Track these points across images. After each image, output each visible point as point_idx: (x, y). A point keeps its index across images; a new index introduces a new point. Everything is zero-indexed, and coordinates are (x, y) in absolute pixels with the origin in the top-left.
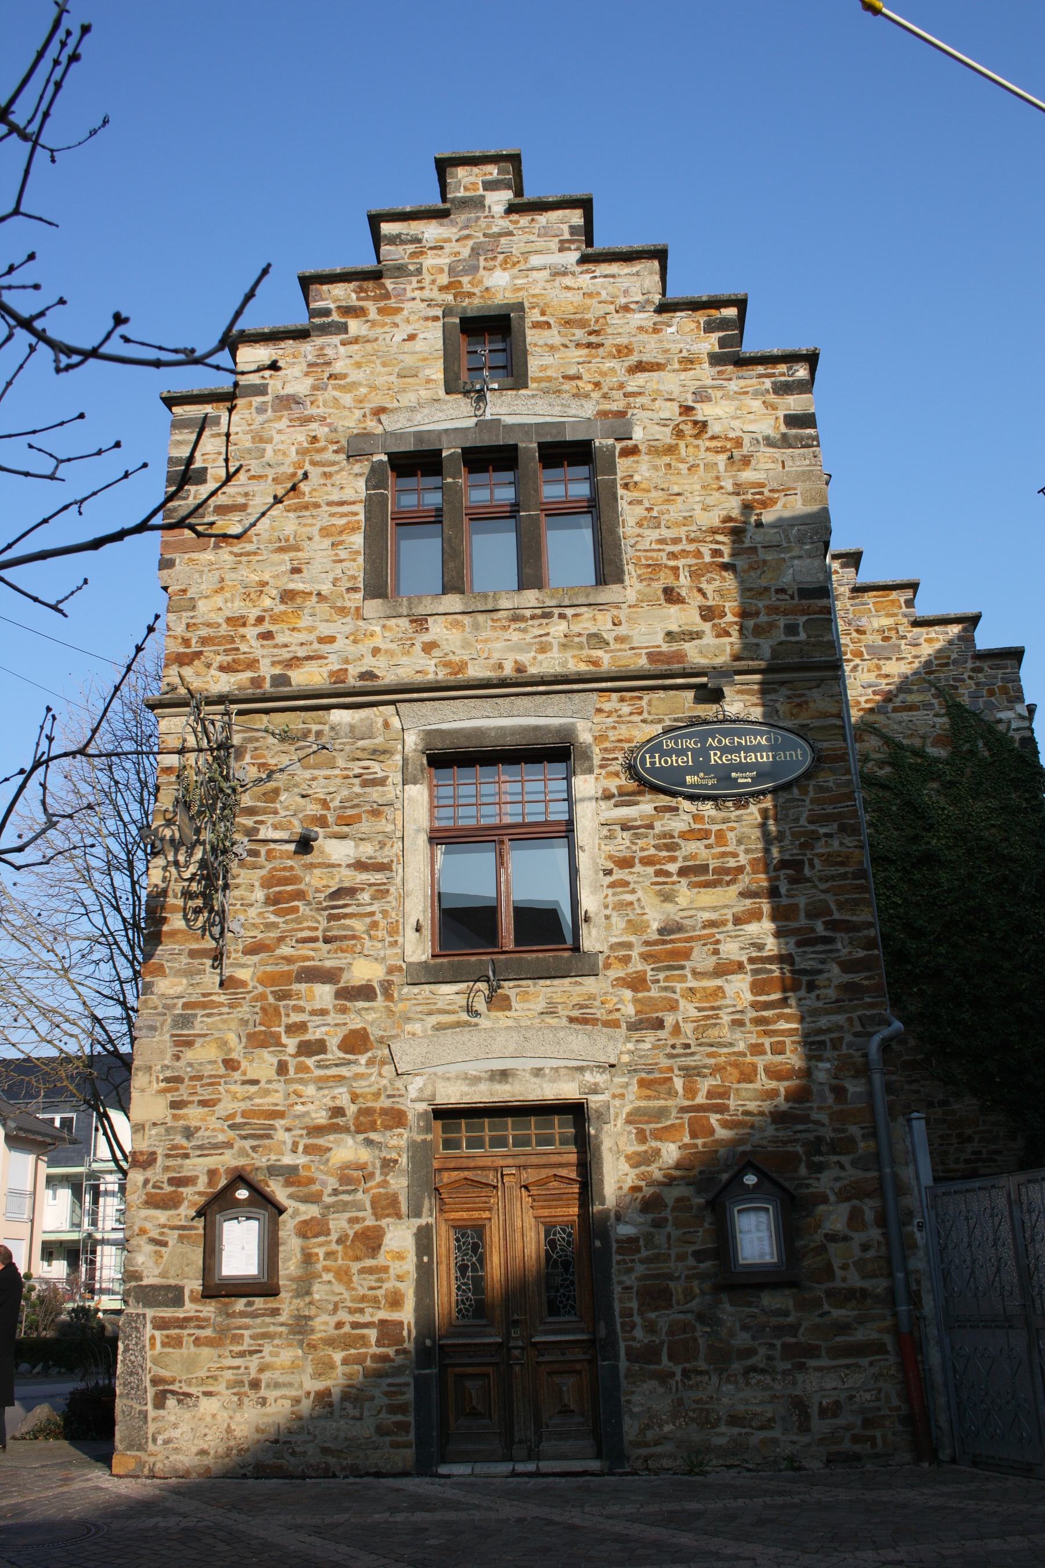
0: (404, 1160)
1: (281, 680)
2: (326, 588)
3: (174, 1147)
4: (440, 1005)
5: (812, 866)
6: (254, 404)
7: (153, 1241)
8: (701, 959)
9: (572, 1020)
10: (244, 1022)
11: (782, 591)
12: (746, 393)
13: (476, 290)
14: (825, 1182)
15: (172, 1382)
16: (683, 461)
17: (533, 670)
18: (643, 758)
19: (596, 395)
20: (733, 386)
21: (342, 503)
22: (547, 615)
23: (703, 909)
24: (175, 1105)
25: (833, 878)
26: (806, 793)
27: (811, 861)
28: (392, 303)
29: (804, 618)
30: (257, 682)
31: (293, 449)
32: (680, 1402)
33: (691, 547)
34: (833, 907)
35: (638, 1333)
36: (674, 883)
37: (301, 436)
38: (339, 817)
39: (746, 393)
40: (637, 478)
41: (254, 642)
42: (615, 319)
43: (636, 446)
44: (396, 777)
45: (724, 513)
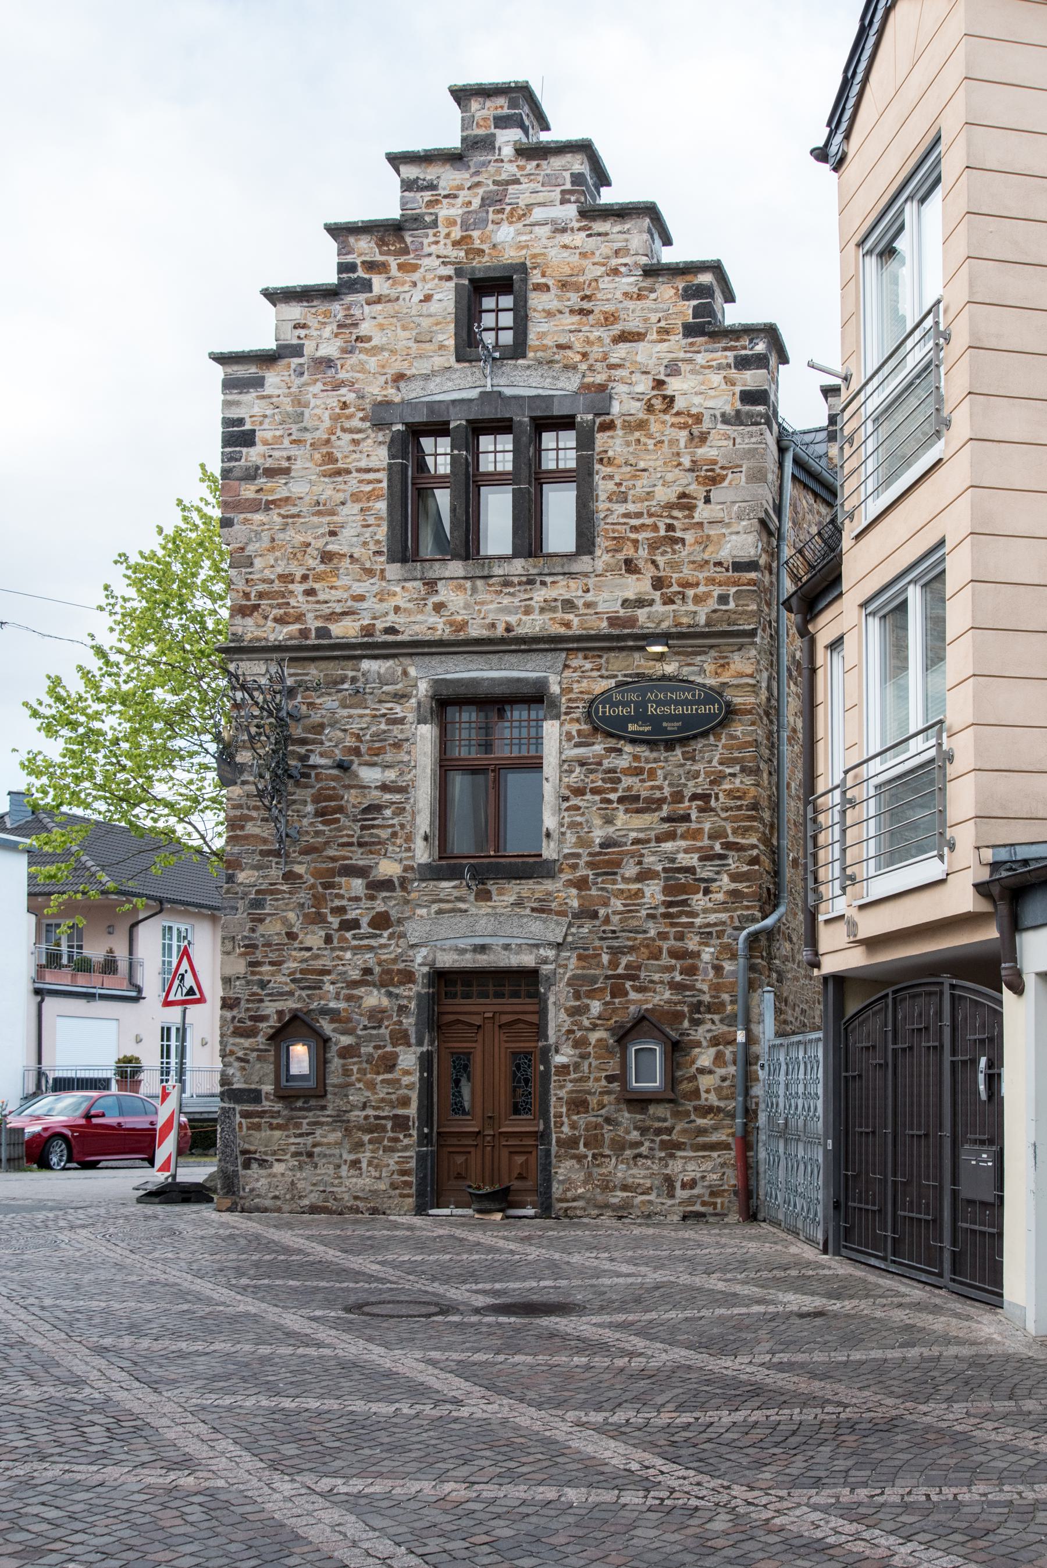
0: (413, 1006)
1: (323, 633)
2: (357, 552)
3: (254, 994)
4: (442, 896)
5: (717, 799)
6: (293, 366)
7: (239, 1059)
8: (630, 870)
9: (533, 910)
10: (302, 906)
11: (719, 564)
12: (710, 367)
13: (484, 247)
14: (701, 1033)
15: (255, 1152)
16: (650, 436)
17: (520, 631)
18: (597, 708)
19: (583, 367)
20: (701, 359)
21: (368, 470)
22: (531, 582)
23: (632, 830)
24: (252, 964)
25: (731, 809)
26: (719, 740)
27: (717, 794)
28: (410, 258)
29: (734, 589)
30: (304, 633)
31: (327, 413)
32: (590, 1174)
33: (648, 521)
34: (729, 831)
35: (566, 1129)
36: (613, 809)
37: (332, 401)
38: (369, 749)
39: (710, 367)
40: (610, 453)
41: (301, 598)
42: (605, 283)
43: (612, 421)
44: (411, 717)
45: (681, 489)
